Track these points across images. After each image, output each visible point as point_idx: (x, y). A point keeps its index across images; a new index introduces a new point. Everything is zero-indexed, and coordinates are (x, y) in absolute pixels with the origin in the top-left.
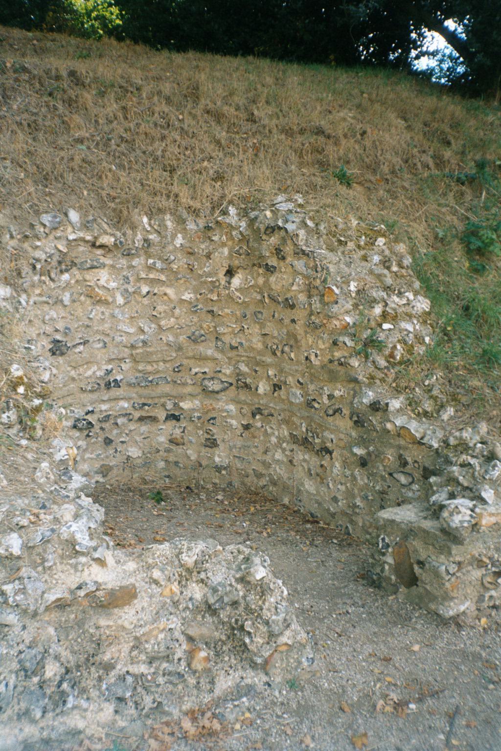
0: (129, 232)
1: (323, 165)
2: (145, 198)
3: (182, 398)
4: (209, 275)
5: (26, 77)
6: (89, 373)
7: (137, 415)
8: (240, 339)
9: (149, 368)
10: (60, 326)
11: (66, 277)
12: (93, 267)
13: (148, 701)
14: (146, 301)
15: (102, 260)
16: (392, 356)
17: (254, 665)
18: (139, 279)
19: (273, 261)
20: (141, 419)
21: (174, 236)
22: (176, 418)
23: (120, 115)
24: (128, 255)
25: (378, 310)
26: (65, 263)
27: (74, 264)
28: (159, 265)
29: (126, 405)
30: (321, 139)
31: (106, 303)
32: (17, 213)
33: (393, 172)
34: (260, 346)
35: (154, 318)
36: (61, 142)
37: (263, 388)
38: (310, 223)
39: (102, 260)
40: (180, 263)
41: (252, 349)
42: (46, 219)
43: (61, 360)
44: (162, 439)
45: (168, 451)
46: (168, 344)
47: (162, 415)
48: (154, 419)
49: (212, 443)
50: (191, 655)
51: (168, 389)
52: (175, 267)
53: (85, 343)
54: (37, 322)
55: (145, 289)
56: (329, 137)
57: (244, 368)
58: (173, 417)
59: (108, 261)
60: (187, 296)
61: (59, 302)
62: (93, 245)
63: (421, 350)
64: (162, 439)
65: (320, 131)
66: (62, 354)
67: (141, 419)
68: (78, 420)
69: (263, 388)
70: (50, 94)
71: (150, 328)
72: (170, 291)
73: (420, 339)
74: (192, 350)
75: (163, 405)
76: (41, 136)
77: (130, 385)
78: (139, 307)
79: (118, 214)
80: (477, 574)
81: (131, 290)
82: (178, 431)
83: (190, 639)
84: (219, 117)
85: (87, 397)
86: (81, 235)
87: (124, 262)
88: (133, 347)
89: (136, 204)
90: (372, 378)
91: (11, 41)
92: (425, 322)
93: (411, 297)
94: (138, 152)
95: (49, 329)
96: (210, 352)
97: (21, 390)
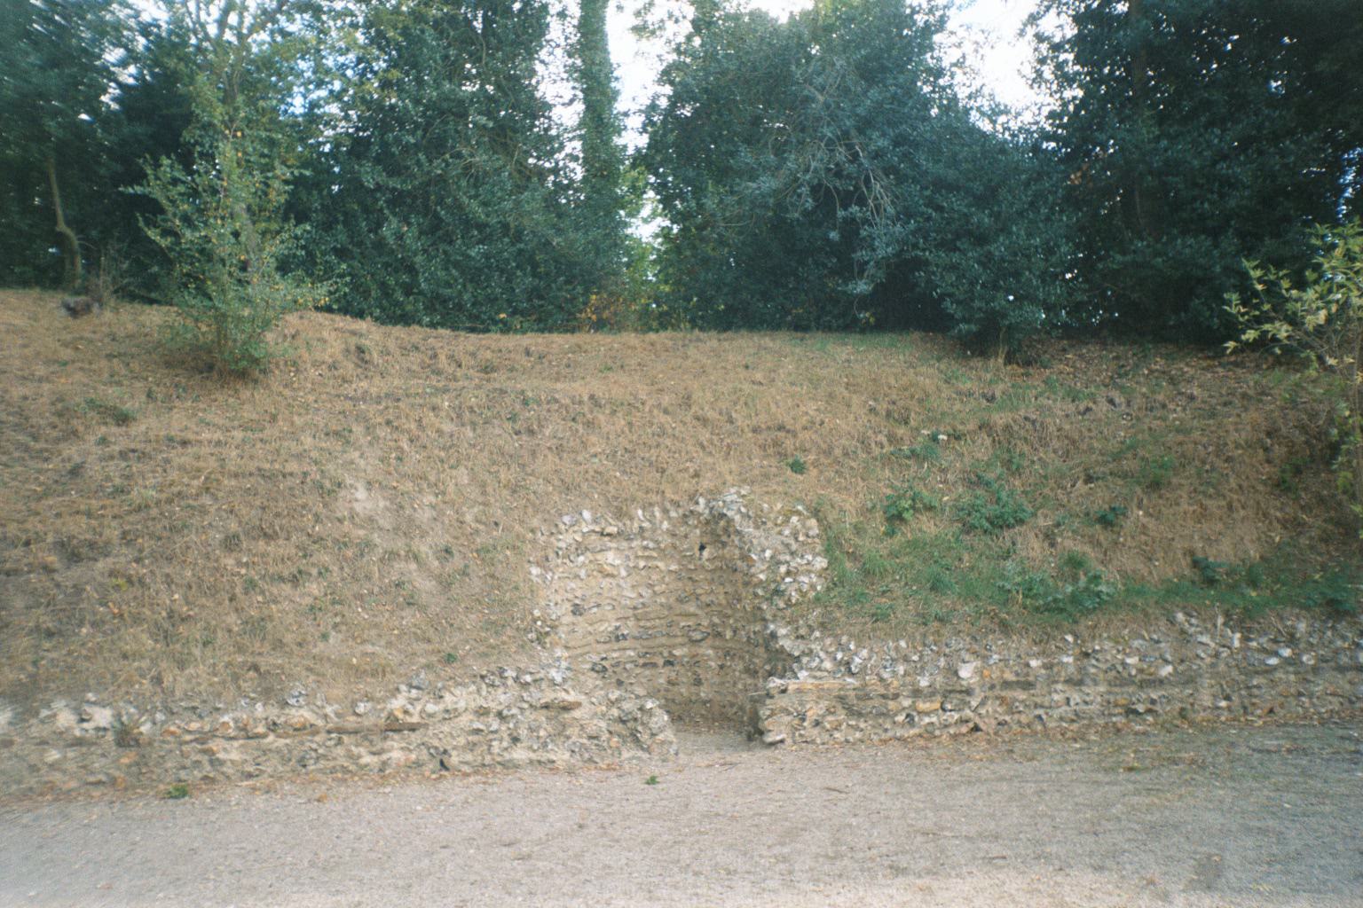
0: (628, 522)
1: (783, 455)
2: (640, 494)
3: (674, 646)
4: (688, 550)
5: (556, 407)
6: (602, 628)
7: (641, 661)
8: (712, 598)
9: (648, 624)
10: (579, 594)
11: (581, 558)
12: (602, 550)
13: (586, 756)
14: (643, 572)
15: (609, 544)
16: (789, 600)
17: (643, 749)
18: (637, 557)
19: (724, 538)
20: (645, 665)
21: (661, 522)
22: (671, 663)
23: (626, 429)
24: (629, 539)
25: (783, 569)
26: (581, 548)
27: (587, 549)
28: (651, 545)
29: (632, 654)
30: (781, 434)
31: (612, 576)
32: (547, 516)
33: (846, 454)
34: (724, 602)
35: (651, 586)
36: (580, 458)
37: (729, 634)
38: (743, 510)
39: (609, 544)
40: (666, 541)
41: (720, 605)
42: (566, 519)
43: (580, 618)
44: (662, 681)
45: (667, 690)
46: (662, 605)
47: (661, 662)
48: (654, 665)
49: (698, 682)
50: (609, 740)
51: (664, 640)
52: (662, 546)
53: (599, 606)
54: (561, 591)
55: (642, 564)
56: (788, 431)
57: (716, 620)
58: (669, 663)
59: (613, 545)
60: (674, 567)
61: (577, 576)
62: (602, 534)
63: (812, 594)
64: (662, 681)
65: (781, 428)
66: (581, 614)
67: (645, 665)
68: (595, 664)
69: (729, 634)
70: (574, 420)
71: (647, 593)
72: (661, 565)
73: (813, 587)
74: (679, 608)
75: (661, 653)
76: (565, 455)
77: (635, 638)
78: (638, 578)
79: (619, 509)
80: (787, 719)
81: (631, 565)
82: (673, 674)
83: (610, 733)
84: (703, 421)
85: (601, 647)
86: (592, 527)
87: (625, 544)
88: (635, 608)
89: (633, 500)
90: (775, 616)
91: (551, 357)
92: (820, 576)
93: (810, 558)
94: (639, 460)
95: (570, 596)
96: (692, 609)
97: (539, 623)
